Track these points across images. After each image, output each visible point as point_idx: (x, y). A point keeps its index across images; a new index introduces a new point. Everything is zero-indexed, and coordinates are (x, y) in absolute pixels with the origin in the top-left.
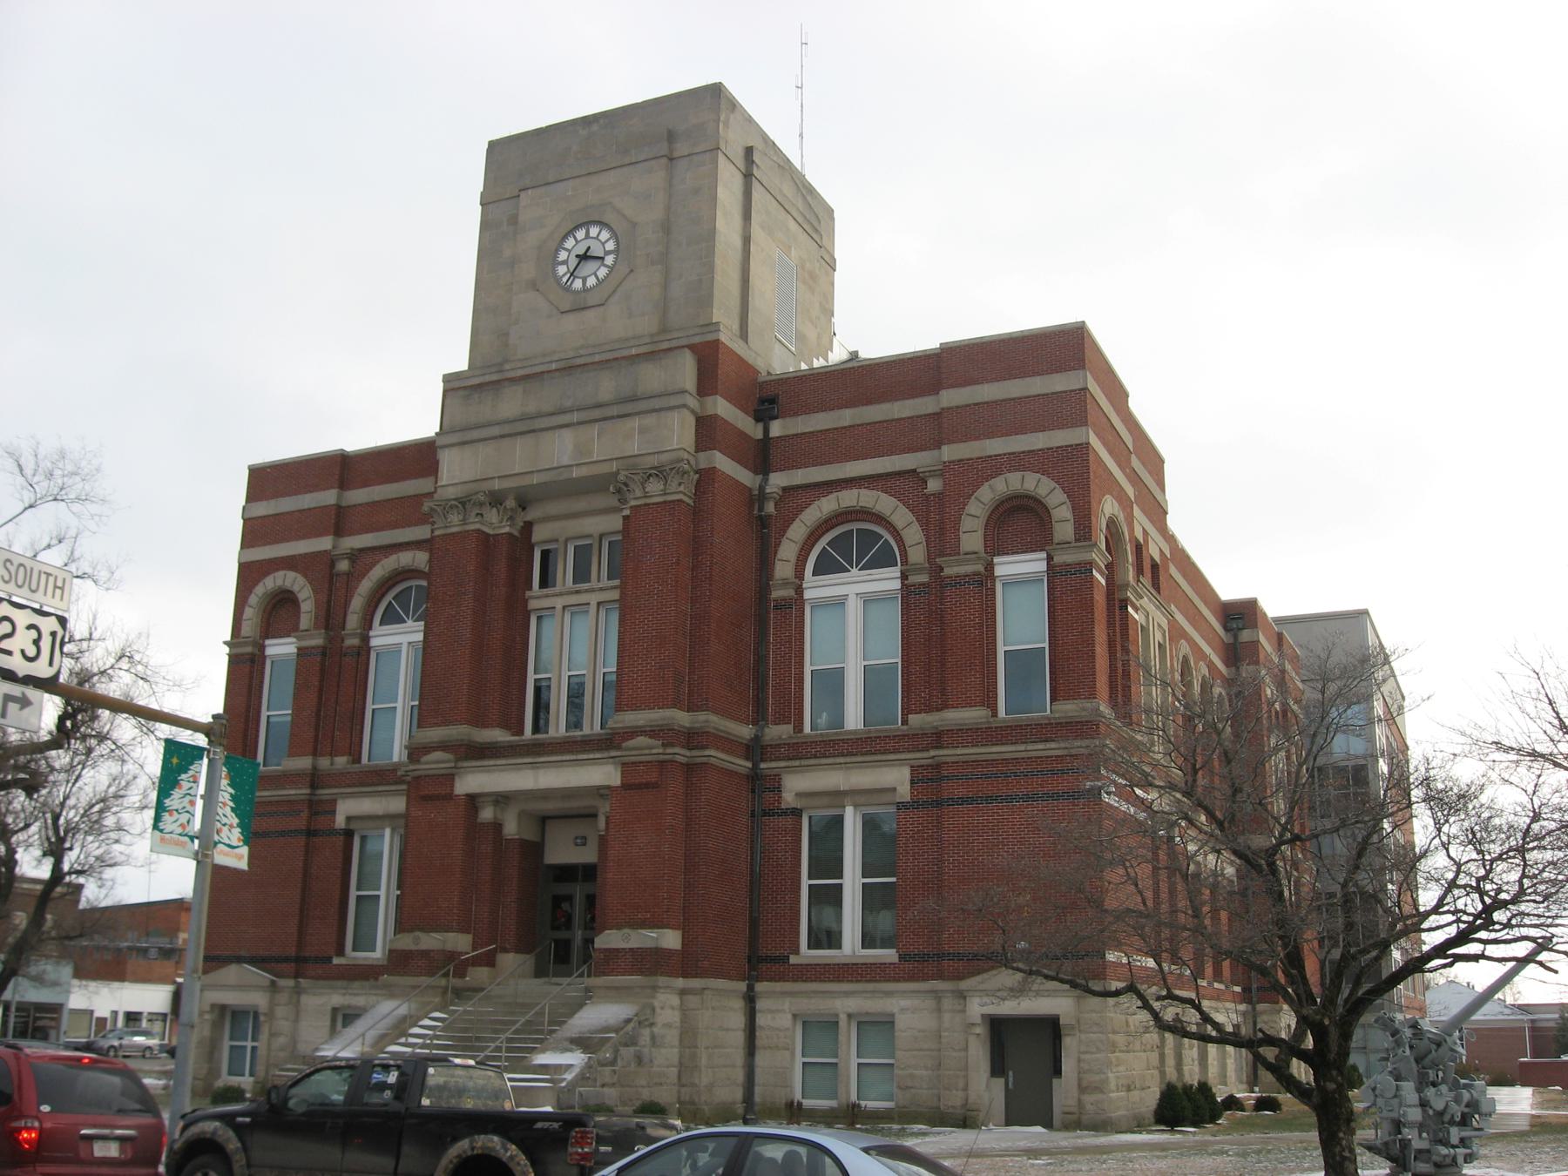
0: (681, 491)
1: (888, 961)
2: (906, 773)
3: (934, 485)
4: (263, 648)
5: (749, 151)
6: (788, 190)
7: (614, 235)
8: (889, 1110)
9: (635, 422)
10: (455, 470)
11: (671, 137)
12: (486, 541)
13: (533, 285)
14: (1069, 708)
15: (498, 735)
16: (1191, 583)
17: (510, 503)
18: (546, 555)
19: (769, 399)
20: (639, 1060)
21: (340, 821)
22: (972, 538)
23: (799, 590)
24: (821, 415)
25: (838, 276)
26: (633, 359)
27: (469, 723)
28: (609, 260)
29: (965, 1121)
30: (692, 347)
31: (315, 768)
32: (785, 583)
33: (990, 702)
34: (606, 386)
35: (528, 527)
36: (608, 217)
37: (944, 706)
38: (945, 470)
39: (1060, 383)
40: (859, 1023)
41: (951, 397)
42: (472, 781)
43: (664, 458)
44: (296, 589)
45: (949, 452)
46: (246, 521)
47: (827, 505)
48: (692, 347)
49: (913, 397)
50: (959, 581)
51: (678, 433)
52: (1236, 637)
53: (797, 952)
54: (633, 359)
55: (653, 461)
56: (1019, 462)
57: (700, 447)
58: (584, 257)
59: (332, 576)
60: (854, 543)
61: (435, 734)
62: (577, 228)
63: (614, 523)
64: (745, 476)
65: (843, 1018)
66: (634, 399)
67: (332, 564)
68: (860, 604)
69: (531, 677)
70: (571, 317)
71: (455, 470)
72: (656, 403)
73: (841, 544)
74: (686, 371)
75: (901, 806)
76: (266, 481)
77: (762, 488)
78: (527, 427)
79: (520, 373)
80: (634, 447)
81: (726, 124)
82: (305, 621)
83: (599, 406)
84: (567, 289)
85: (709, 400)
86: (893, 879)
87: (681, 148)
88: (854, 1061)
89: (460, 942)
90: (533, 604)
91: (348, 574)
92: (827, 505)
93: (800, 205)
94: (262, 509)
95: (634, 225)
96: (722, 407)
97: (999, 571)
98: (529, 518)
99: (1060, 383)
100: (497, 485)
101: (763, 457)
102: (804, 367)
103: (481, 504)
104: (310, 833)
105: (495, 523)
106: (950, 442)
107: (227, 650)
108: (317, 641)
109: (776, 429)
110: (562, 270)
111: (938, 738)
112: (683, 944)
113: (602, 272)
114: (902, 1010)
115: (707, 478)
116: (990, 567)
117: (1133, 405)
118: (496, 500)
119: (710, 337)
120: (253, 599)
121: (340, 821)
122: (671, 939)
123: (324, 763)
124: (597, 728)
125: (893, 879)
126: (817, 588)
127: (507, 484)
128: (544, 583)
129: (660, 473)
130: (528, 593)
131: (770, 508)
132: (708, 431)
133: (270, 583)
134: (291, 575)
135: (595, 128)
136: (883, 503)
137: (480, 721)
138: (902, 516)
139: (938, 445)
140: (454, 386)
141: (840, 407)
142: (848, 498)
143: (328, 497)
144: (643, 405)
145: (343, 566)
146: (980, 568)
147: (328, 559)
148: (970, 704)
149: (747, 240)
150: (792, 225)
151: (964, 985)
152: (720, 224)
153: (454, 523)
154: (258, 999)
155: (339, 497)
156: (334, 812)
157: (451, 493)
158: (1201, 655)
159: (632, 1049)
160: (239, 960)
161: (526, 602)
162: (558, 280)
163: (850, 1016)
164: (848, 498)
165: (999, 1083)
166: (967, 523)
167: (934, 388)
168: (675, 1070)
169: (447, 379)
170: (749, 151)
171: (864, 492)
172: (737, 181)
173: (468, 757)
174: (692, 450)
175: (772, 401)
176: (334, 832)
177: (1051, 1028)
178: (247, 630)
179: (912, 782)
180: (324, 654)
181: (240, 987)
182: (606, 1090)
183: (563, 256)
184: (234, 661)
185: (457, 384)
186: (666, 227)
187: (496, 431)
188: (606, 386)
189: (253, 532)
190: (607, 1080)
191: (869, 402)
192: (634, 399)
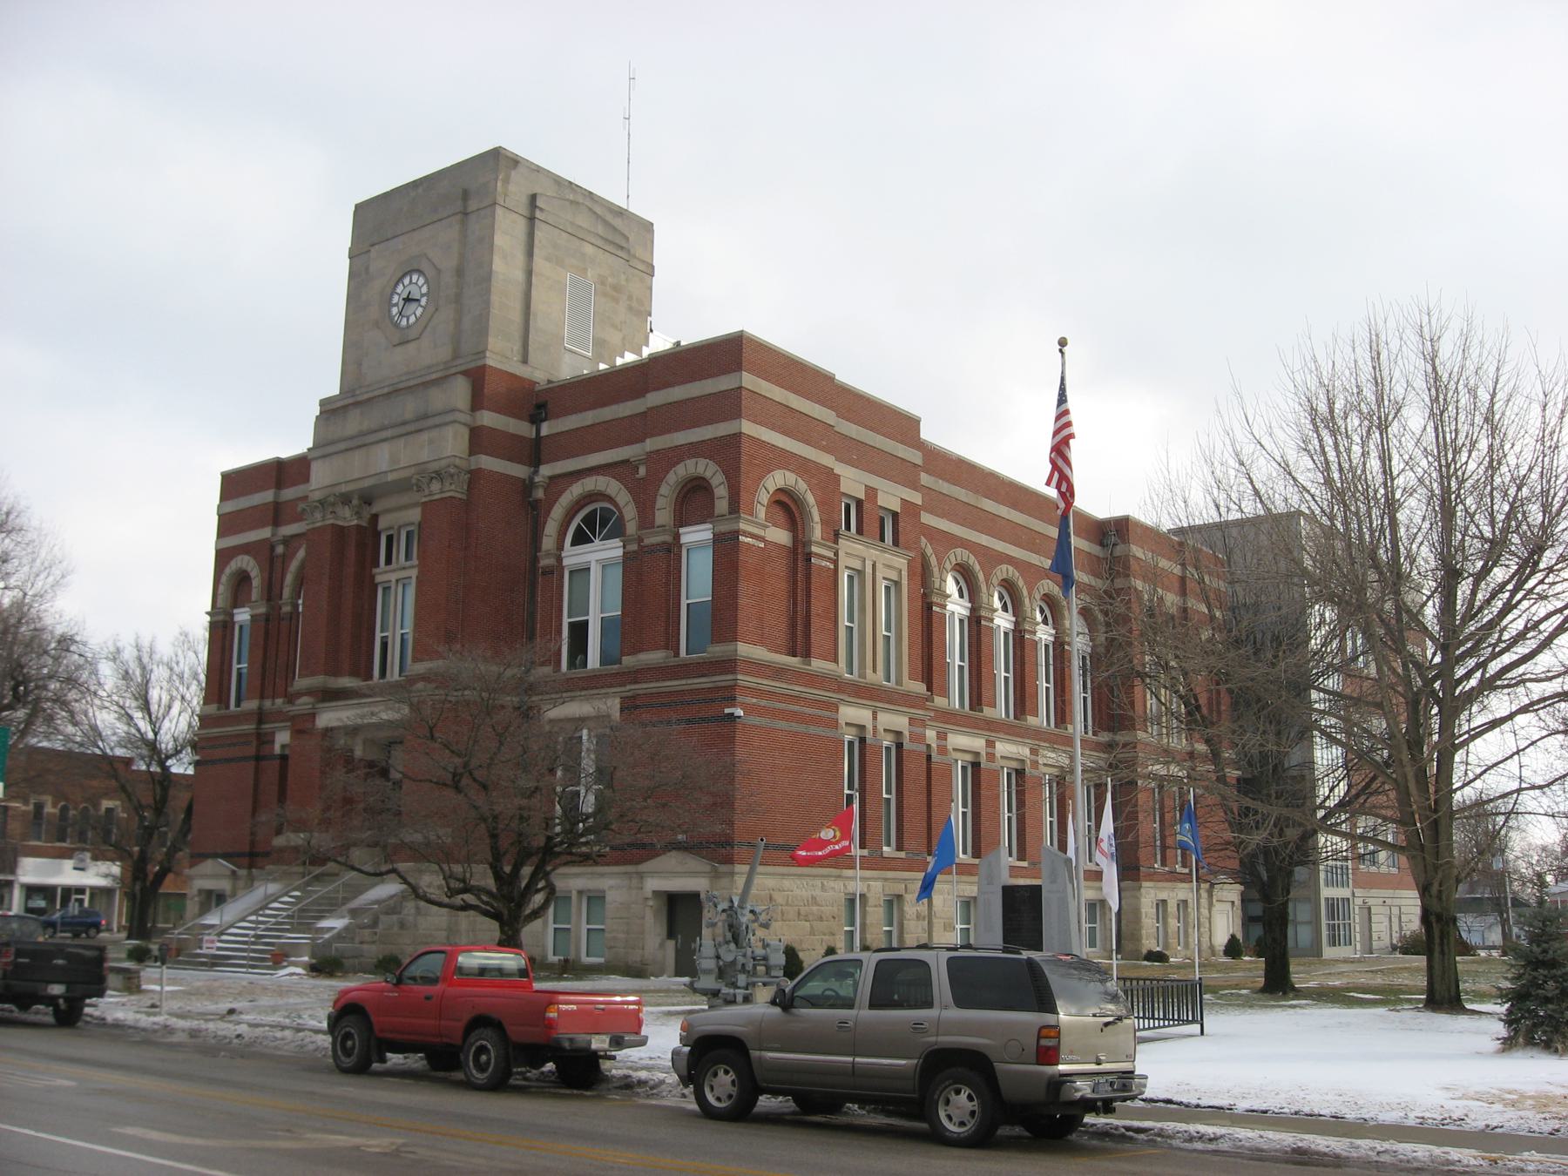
0: (455, 490)
2: (618, 701)
3: (642, 471)
4: (232, 615)
5: (533, 198)
6: (584, 220)
7: (427, 282)
8: (600, 965)
9: (425, 436)
10: (321, 477)
11: (466, 195)
12: (340, 532)
13: (377, 325)
14: (717, 650)
15: (347, 682)
16: (1014, 505)
17: (355, 502)
18: (390, 539)
19: (538, 403)
20: (402, 925)
21: (277, 749)
22: (663, 515)
23: (560, 559)
24: (574, 417)
25: (658, 282)
26: (426, 385)
27: (326, 674)
28: (424, 301)
29: (637, 972)
30: (465, 373)
31: (260, 708)
32: (548, 554)
33: (672, 644)
34: (409, 407)
35: (375, 518)
36: (425, 266)
37: (641, 650)
38: (652, 457)
39: (723, 383)
40: (589, 898)
41: (655, 399)
42: (329, 717)
43: (443, 463)
44: (708, 475)
45: (651, 444)
46: (220, 516)
47: (577, 490)
48: (465, 373)
49: (633, 398)
50: (653, 549)
51: (451, 444)
54: (426, 385)
55: (435, 466)
56: (695, 450)
57: (472, 452)
58: (408, 300)
59: (272, 559)
60: (595, 523)
61: (421, 668)
62: (404, 276)
63: (415, 515)
64: (519, 471)
65: (574, 894)
66: (426, 417)
67: (272, 548)
68: (599, 569)
69: (378, 635)
70: (399, 349)
71: (321, 477)
72: (437, 420)
73: (589, 520)
74: (459, 393)
76: (234, 483)
77: (531, 479)
78: (360, 442)
79: (366, 396)
80: (424, 456)
81: (507, 181)
82: (255, 595)
83: (404, 423)
84: (396, 325)
85: (478, 414)
87: (473, 205)
88: (584, 927)
89: (323, 840)
90: (379, 579)
91: (284, 555)
92: (577, 490)
93: (600, 230)
94: (231, 506)
96: (488, 418)
97: (684, 539)
98: (374, 511)
99: (723, 383)
100: (344, 488)
101: (535, 452)
102: (602, 366)
103: (333, 504)
104: (258, 758)
105: (347, 517)
106: (652, 436)
107: (208, 618)
108: (262, 610)
109: (546, 429)
110: (395, 310)
111: (636, 675)
113: (419, 311)
114: (611, 887)
115: (475, 475)
116: (677, 536)
118: (345, 499)
119: (480, 363)
120: (224, 579)
121: (277, 749)
123: (268, 703)
124: (396, 677)
126: (573, 556)
127: (351, 487)
128: (389, 561)
129: (438, 475)
130: (375, 571)
131: (539, 494)
132: (479, 440)
133: (234, 565)
134: (702, 462)
135: (420, 190)
136: (611, 486)
137: (336, 673)
138: (623, 497)
139: (642, 440)
140: (330, 411)
143: (267, 496)
144: (430, 422)
145: (280, 549)
146: (668, 538)
147: (269, 545)
148: (656, 647)
149: (529, 273)
150: (589, 249)
151: (643, 867)
152: (498, 265)
153: (318, 520)
154: (224, 885)
155: (276, 495)
156: (273, 742)
157: (317, 496)
159: (395, 917)
160: (215, 856)
161: (373, 577)
162: (391, 317)
163: (580, 893)
165: (671, 944)
167: (641, 393)
168: (444, 934)
169: (323, 403)
170: (533, 198)
171: (601, 478)
172: (521, 225)
173: (323, 701)
174: (465, 455)
175: (541, 406)
176: (272, 757)
177: (695, 896)
178: (220, 604)
179: (622, 710)
180: (267, 620)
181: (215, 876)
182: (365, 946)
183: (396, 299)
184: (213, 626)
185: (329, 407)
186: (460, 272)
187: (342, 446)
188: (409, 407)
189: (227, 524)
190: (367, 938)
191: (604, 405)
192: (426, 417)
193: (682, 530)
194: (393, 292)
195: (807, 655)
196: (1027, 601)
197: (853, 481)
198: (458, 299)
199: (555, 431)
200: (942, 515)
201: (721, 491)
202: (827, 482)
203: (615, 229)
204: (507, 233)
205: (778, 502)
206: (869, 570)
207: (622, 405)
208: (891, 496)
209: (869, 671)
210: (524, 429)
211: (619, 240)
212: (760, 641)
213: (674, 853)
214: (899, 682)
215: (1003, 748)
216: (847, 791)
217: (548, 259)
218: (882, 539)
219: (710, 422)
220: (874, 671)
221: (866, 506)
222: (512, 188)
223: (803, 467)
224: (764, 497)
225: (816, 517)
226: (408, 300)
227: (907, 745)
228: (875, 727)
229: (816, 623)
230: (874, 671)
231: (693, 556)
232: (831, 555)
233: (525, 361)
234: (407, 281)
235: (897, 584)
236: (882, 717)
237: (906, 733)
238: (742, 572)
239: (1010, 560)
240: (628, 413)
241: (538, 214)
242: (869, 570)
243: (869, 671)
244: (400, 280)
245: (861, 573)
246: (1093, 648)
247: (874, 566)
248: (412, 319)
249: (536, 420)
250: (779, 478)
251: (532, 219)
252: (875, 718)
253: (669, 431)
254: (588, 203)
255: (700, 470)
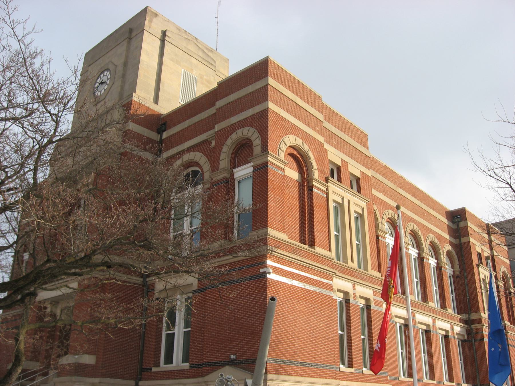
1: (186, 368)
3: (213, 143)
5: (164, 33)
6: (192, 48)
7: (110, 73)
14: (254, 235)
16: (413, 195)
22: (224, 162)
39: (258, 85)
41: (219, 104)
52: (458, 225)
53: (158, 365)
56: (242, 124)
58: (102, 83)
75: (194, 292)
81: (151, 21)
86: (189, 329)
87: (134, 34)
93: (201, 54)
95: (116, 66)
96: (132, 126)
97: (236, 176)
109: (165, 135)
112: (96, 362)
116: (232, 174)
117: (325, 100)
122: (88, 359)
125: (189, 329)
132: (127, 135)
141: (185, 120)
142: (186, 157)
158: (439, 237)
164: (186, 157)
166: (223, 156)
170: (164, 33)
186: (125, 64)
193: (235, 170)
194: (96, 82)
195: (312, 244)
196: (423, 243)
197: (335, 155)
198: (124, 76)
199: (169, 135)
200: (380, 192)
201: (257, 142)
202: (322, 152)
203: (208, 56)
204: (149, 46)
205: (291, 155)
206: (346, 204)
207: (203, 113)
208: (355, 168)
209: (349, 260)
210: (154, 136)
211: (212, 62)
212: (283, 230)
213: (227, 367)
214: (366, 269)
215: (419, 317)
216: (340, 332)
217: (172, 60)
218: (352, 188)
219: (251, 107)
220: (352, 261)
221: (342, 169)
222: (153, 24)
223: (306, 137)
224: (284, 148)
225: (315, 166)
226: (102, 83)
227: (373, 307)
228: (354, 294)
229: (317, 227)
230: (352, 261)
231: (242, 185)
232: (325, 189)
233: (156, 101)
234: (102, 76)
235: (362, 216)
236: (359, 288)
237: (372, 299)
238: (270, 187)
239: (414, 221)
240: (206, 116)
241: (167, 38)
242: (346, 204)
243: (349, 260)
244: (100, 76)
245: (341, 205)
246: (454, 272)
247: (349, 202)
248: (103, 91)
249: (160, 132)
250: (291, 140)
251: (163, 41)
252: (354, 288)
253: (228, 118)
254: (195, 41)
255: (245, 133)
